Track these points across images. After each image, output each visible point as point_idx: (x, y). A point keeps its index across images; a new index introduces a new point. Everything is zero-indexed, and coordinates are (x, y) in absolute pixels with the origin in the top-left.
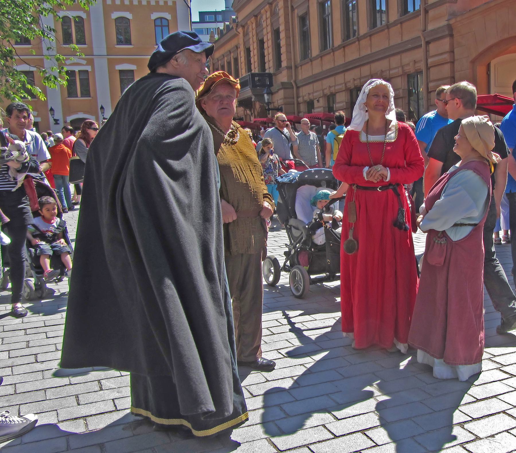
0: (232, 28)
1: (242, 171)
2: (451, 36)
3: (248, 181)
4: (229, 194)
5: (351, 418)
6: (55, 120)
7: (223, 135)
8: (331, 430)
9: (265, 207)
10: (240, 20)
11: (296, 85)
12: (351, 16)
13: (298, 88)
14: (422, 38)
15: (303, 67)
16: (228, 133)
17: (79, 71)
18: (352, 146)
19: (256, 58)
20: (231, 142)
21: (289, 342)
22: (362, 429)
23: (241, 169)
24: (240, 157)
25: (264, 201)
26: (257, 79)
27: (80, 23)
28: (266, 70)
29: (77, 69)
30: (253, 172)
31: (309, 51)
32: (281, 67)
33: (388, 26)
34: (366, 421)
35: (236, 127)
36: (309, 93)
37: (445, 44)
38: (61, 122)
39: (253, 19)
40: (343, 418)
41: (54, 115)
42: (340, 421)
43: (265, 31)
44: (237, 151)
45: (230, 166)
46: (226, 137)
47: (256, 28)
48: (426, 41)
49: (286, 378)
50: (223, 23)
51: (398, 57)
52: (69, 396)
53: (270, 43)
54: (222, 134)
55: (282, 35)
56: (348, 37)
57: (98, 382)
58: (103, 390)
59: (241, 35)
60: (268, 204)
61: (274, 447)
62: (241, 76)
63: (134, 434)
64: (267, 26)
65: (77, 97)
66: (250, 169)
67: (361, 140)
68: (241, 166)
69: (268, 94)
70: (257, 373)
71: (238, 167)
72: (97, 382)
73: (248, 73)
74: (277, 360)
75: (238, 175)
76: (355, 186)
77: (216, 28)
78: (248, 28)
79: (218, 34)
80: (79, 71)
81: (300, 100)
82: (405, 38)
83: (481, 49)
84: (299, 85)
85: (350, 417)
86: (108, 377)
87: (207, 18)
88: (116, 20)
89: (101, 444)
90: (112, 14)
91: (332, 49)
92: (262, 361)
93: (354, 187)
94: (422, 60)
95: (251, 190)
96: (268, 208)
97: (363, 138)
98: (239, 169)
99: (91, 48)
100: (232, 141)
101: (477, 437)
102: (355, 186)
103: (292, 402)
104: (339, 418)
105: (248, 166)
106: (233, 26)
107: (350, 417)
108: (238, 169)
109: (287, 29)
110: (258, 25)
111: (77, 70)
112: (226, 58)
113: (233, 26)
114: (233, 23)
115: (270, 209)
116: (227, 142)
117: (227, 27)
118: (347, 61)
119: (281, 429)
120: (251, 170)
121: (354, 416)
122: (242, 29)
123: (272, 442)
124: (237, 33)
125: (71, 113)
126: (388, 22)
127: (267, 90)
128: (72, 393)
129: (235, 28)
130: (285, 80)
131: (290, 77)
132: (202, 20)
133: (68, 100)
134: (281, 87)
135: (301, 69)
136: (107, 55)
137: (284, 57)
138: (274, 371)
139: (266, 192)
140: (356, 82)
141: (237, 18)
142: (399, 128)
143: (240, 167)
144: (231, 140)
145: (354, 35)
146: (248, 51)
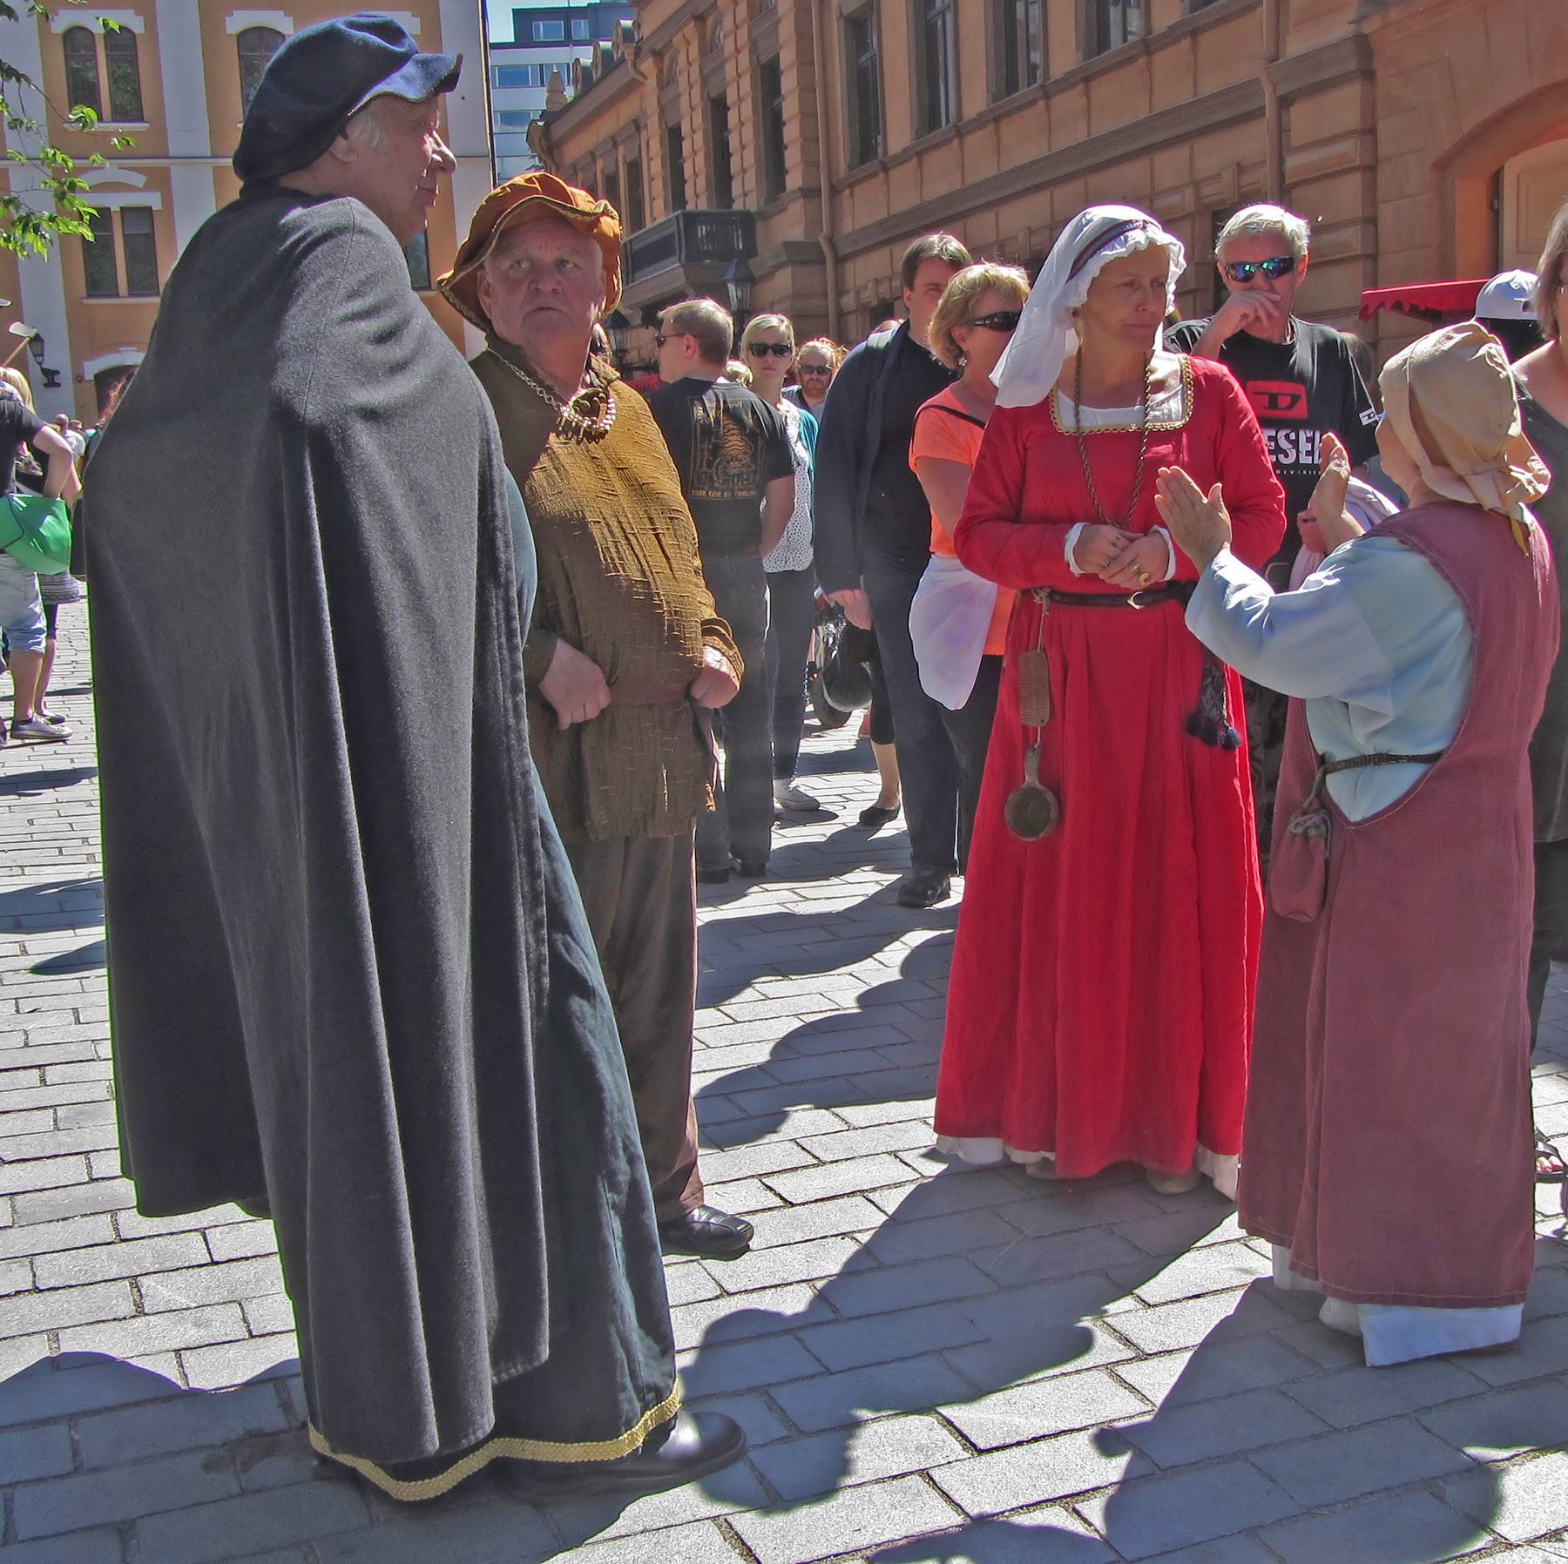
0: (622, 60)
1: (627, 538)
2: (1368, 75)
3: (648, 573)
4: (581, 619)
5: (1026, 1447)
6: (46, 372)
7: (558, 406)
8: (951, 1494)
9: (710, 669)
10: (646, 31)
11: (834, 250)
12: (1020, 15)
13: (840, 261)
14: (1267, 87)
15: (857, 189)
16: (574, 398)
17: (122, 209)
18: (1026, 450)
19: (700, 160)
20: (585, 431)
21: (804, 1149)
22: (1066, 1493)
23: (623, 529)
24: (619, 487)
25: (704, 645)
26: (702, 230)
27: (122, 44)
28: (733, 201)
29: (115, 202)
30: (667, 541)
31: (879, 137)
32: (785, 190)
33: (1149, 46)
34: (1079, 1461)
35: (605, 379)
36: (876, 279)
37: (1344, 108)
38: (66, 378)
39: (690, 29)
40: (994, 1445)
41: (42, 355)
42: (986, 1458)
43: (730, 69)
44: (606, 464)
45: (584, 517)
46: (568, 412)
47: (701, 59)
48: (1279, 93)
49: (791, 1284)
50: (591, 48)
51: (1180, 154)
52: (28, 1335)
53: (747, 109)
54: (554, 403)
55: (789, 82)
56: (1011, 84)
57: (131, 1284)
58: (146, 1314)
59: (651, 83)
60: (718, 655)
61: (741, 1555)
62: (652, 222)
63: (242, 1488)
64: (738, 51)
65: (117, 295)
66: (654, 529)
67: (1059, 426)
68: (622, 519)
69: (738, 282)
70: (687, 1262)
71: (614, 524)
72: (127, 1283)
73: (674, 211)
74: (759, 1215)
75: (613, 550)
76: (1043, 594)
77: (568, 65)
78: (674, 60)
79: (576, 82)
80: (122, 209)
81: (848, 301)
82: (1209, 87)
83: (1472, 120)
84: (845, 250)
85: (1020, 1443)
86: (168, 1265)
87: (541, 29)
88: (241, 36)
89: (124, 1522)
90: (227, 18)
91: (956, 126)
92: (703, 1218)
93: (1041, 598)
94: (1265, 161)
95: (660, 606)
96: (718, 671)
97: (1065, 419)
98: (617, 531)
99: (161, 132)
100: (589, 426)
101: (1496, 1539)
102: (1043, 594)
103: (812, 1377)
104: (982, 1446)
105: (646, 521)
106: (623, 54)
107: (1020, 1443)
108: (613, 528)
109: (804, 61)
110: (709, 48)
111: (115, 208)
112: (600, 164)
113: (623, 54)
114: (624, 41)
115: (724, 674)
116: (570, 430)
117: (608, 62)
118: (1005, 167)
119: (769, 1483)
120: (657, 536)
121: (1035, 1440)
122: (655, 63)
123: (736, 1533)
124: (637, 77)
125: (97, 350)
126: (1148, 30)
127: (737, 269)
128: (37, 1323)
129: (629, 58)
130: (796, 233)
131: (813, 222)
132: (524, 38)
133: (88, 306)
134: (784, 258)
135: (852, 195)
136: (213, 157)
137: (792, 157)
138: (746, 1256)
139: (709, 613)
140: (1035, 240)
141: (637, 25)
142: (1196, 380)
143: (620, 522)
144: (587, 423)
145: (1032, 78)
146: (674, 137)
